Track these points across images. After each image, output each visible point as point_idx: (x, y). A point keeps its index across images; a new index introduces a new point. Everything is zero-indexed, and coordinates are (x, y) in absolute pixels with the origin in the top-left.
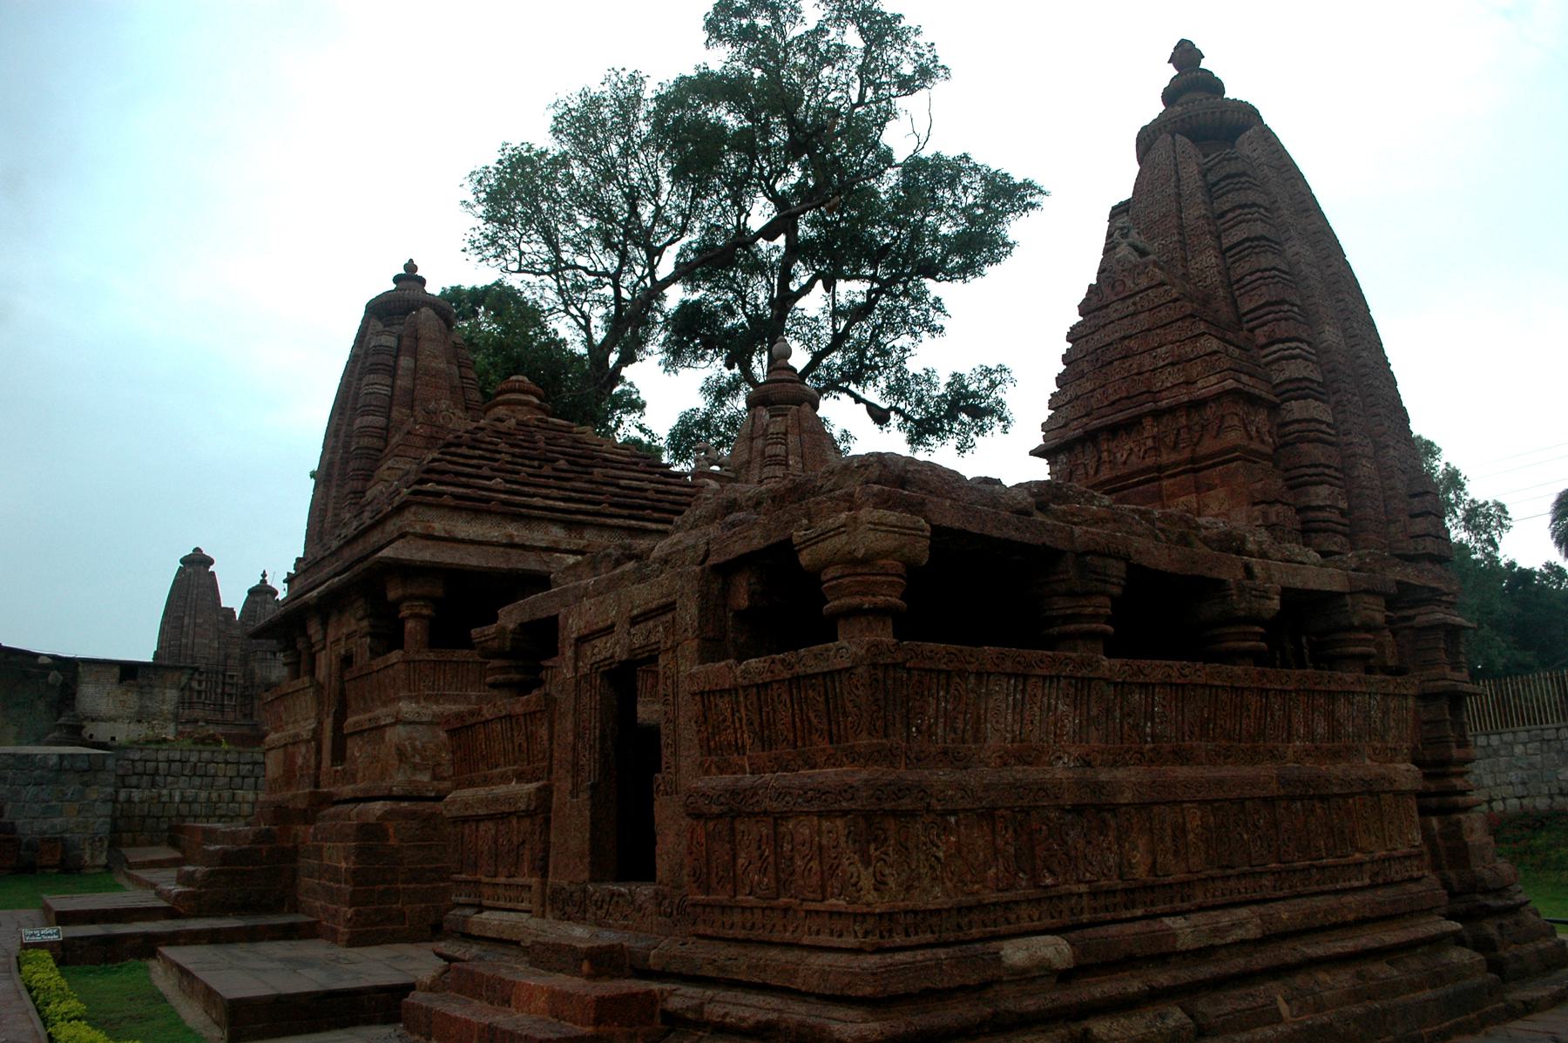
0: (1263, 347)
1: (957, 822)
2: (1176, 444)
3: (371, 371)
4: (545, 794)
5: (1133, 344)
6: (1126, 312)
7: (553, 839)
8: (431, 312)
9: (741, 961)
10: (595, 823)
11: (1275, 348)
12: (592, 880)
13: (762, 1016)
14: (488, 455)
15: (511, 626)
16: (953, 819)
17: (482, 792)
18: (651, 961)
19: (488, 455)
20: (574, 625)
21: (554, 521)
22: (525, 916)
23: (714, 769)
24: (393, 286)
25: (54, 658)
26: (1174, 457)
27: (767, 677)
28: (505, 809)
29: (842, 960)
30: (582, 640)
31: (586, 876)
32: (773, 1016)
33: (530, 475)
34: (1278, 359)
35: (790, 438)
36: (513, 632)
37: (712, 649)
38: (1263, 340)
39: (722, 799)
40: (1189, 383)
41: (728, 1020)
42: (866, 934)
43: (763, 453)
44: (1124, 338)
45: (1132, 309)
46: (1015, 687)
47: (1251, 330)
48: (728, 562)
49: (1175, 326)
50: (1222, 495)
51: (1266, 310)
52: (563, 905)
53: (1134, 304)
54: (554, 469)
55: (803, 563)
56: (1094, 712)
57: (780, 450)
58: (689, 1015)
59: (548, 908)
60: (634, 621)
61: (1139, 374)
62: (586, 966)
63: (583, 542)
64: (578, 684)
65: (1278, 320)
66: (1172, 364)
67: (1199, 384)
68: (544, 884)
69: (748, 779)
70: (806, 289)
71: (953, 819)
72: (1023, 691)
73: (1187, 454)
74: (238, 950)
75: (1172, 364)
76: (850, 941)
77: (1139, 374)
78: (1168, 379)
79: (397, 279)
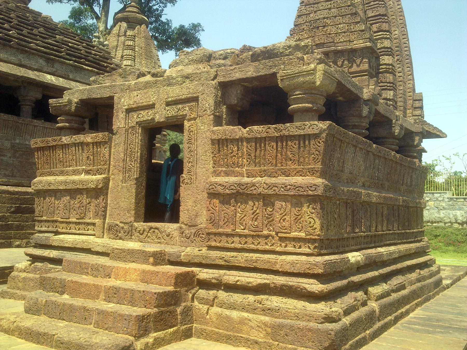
0: (375, 32)
1: (339, 203)
4: (106, 181)
5: (328, 21)
6: (327, 7)
9: (241, 258)
10: (137, 195)
11: (380, 33)
12: (135, 221)
15: (76, 100)
18: (182, 257)
19: (6, 18)
20: (123, 102)
21: (42, 57)
22: (92, 237)
23: (222, 174)
27: (264, 135)
28: (81, 187)
29: (304, 258)
30: (129, 111)
31: (132, 219)
33: (28, 32)
34: (383, 38)
36: (77, 103)
37: (218, 121)
38: (375, 29)
39: (232, 187)
41: (238, 283)
42: (315, 248)
44: (324, 18)
45: (329, 6)
48: (231, 81)
49: (347, 17)
51: (379, 17)
52: (113, 231)
54: (39, 32)
57: (131, 43)
58: (213, 281)
59: (105, 235)
60: (168, 104)
61: (330, 34)
62: (151, 260)
63: (54, 70)
64: (127, 131)
65: (383, 22)
66: (345, 32)
67: (355, 42)
68: (104, 223)
75: (345, 32)
76: (307, 250)
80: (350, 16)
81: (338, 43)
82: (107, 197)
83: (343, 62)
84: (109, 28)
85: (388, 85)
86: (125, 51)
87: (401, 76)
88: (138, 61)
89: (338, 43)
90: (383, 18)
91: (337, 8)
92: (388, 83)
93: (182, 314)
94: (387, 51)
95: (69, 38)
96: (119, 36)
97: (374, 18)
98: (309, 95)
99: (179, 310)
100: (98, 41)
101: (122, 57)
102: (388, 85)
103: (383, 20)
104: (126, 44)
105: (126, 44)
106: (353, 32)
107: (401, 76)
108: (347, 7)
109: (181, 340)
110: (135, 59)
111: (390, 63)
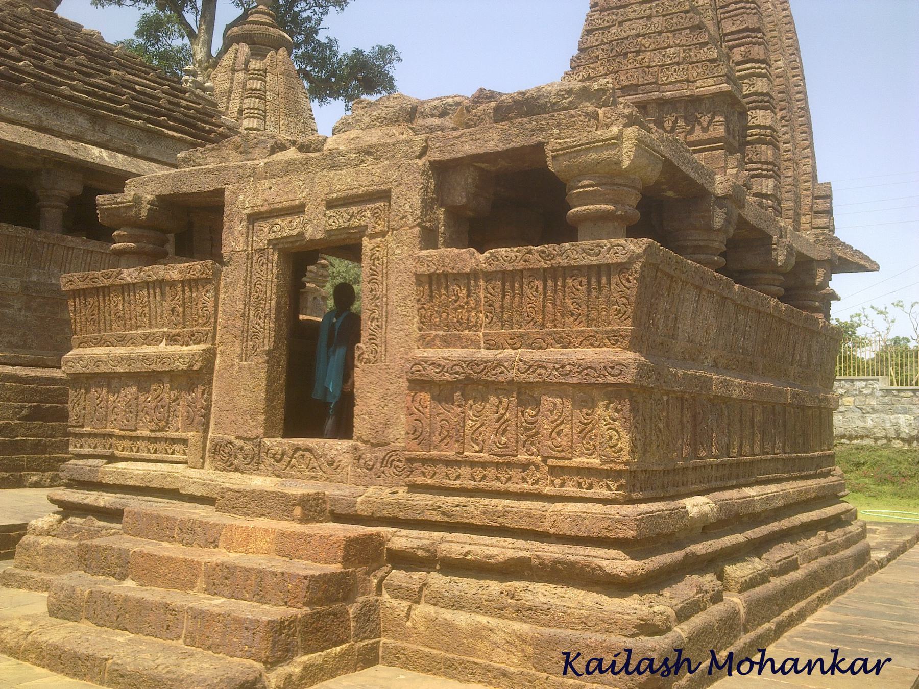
1: (667, 400)
4: (209, 357)
5: (646, 42)
6: (643, 14)
7: (214, 398)
9: (474, 508)
12: (266, 435)
13: (510, 553)
15: (149, 197)
17: (120, 351)
19: (12, 36)
20: (243, 200)
27: (520, 266)
28: (158, 367)
29: (598, 508)
30: (254, 218)
31: (261, 431)
32: (527, 554)
33: (55, 64)
36: (151, 203)
38: (738, 58)
41: (469, 557)
42: (620, 488)
43: (244, 87)
44: (638, 36)
45: (648, 12)
47: (731, 48)
48: (455, 160)
51: (745, 34)
52: (223, 455)
54: (77, 63)
55: (97, 197)
57: (257, 85)
59: (208, 462)
60: (331, 205)
61: (648, 67)
62: (298, 511)
63: (107, 137)
64: (249, 257)
65: (754, 44)
66: (678, 64)
67: (698, 84)
68: (205, 439)
69: (484, 354)
75: (678, 64)
76: (605, 493)
80: (688, 31)
82: (211, 388)
83: (675, 122)
85: (765, 167)
86: (246, 100)
87: (789, 150)
88: (272, 119)
89: (665, 84)
90: (753, 35)
92: (763, 163)
93: (357, 617)
94: (762, 101)
96: (234, 71)
97: (736, 36)
99: (352, 610)
100: (193, 82)
101: (240, 112)
102: (765, 167)
103: (753, 40)
107: (789, 150)
108: (683, 15)
109: (356, 670)
110: (265, 117)
111: (768, 124)
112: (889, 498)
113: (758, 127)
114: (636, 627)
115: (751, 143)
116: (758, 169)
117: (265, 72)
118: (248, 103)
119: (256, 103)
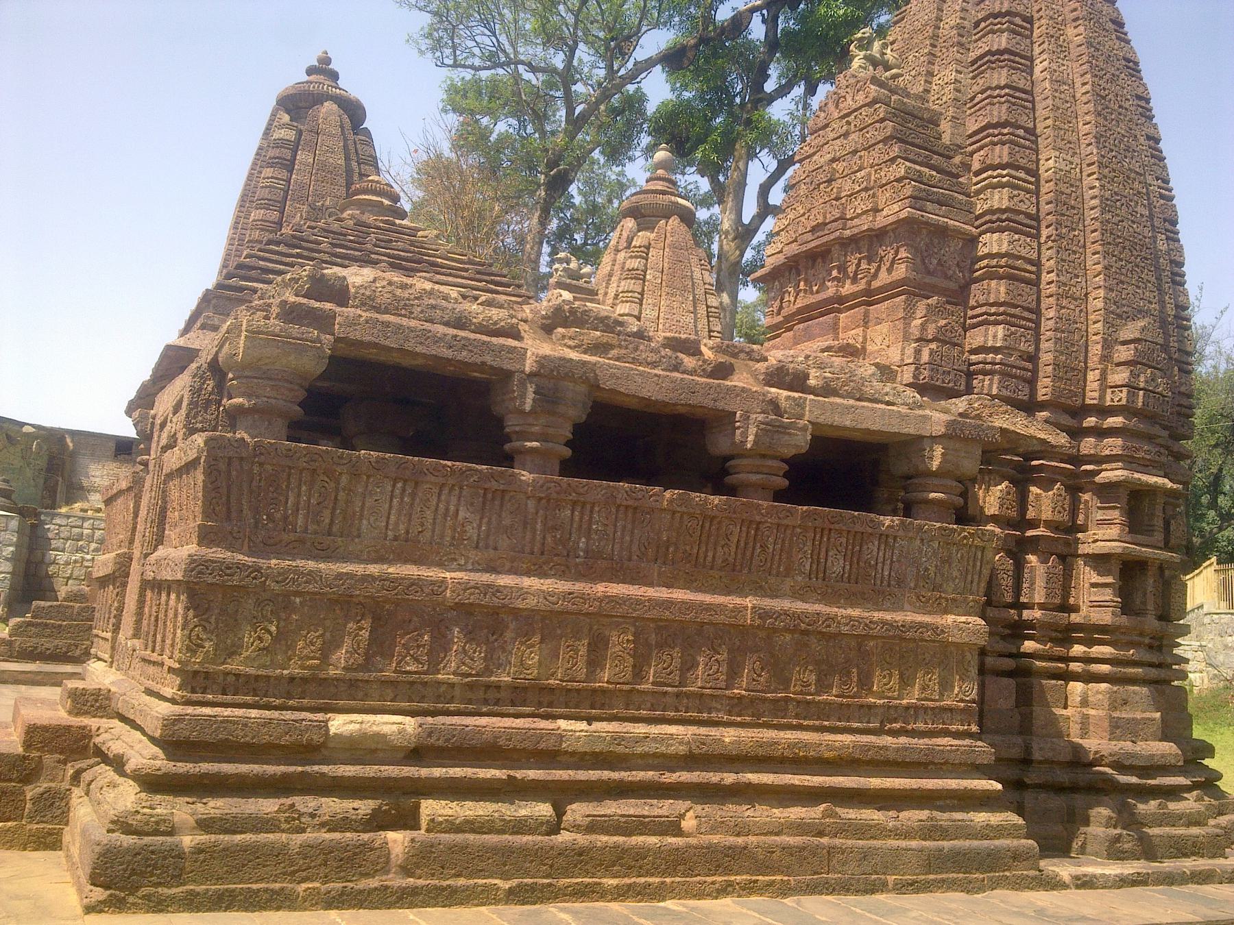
2: (856, 274)
3: (270, 165)
8: (335, 107)
14: (306, 253)
16: (298, 600)
24: (306, 78)
25: (39, 427)
26: (855, 288)
35: (652, 252)
40: (876, 210)
46: (404, 490)
50: (885, 330)
53: (849, 123)
56: (507, 521)
57: (635, 263)
61: (837, 199)
70: (782, 91)
71: (298, 600)
72: (413, 495)
73: (862, 285)
74: (1138, 890)
77: (837, 199)
78: (861, 205)
79: (310, 71)
80: (881, 145)
81: (852, 219)
82: (124, 591)
83: (858, 265)
84: (746, 219)
85: (993, 310)
86: (623, 283)
87: (1052, 282)
88: (650, 301)
89: (852, 219)
90: (996, 132)
91: (861, 130)
92: (992, 305)
93: (35, 801)
94: (999, 220)
95: (450, 275)
96: (617, 251)
97: (974, 139)
98: (244, 381)
99: (31, 792)
100: (565, 270)
101: (616, 296)
102: (993, 310)
103: (996, 139)
104: (627, 267)
105: (627, 267)
106: (884, 185)
107: (1052, 282)
108: (878, 125)
109: (25, 849)
110: (641, 300)
111: (1003, 251)
112: (1082, 784)
113: (990, 256)
114: (112, 822)
115: (977, 280)
116: (982, 315)
117: (648, 248)
118: (624, 285)
119: (634, 285)
